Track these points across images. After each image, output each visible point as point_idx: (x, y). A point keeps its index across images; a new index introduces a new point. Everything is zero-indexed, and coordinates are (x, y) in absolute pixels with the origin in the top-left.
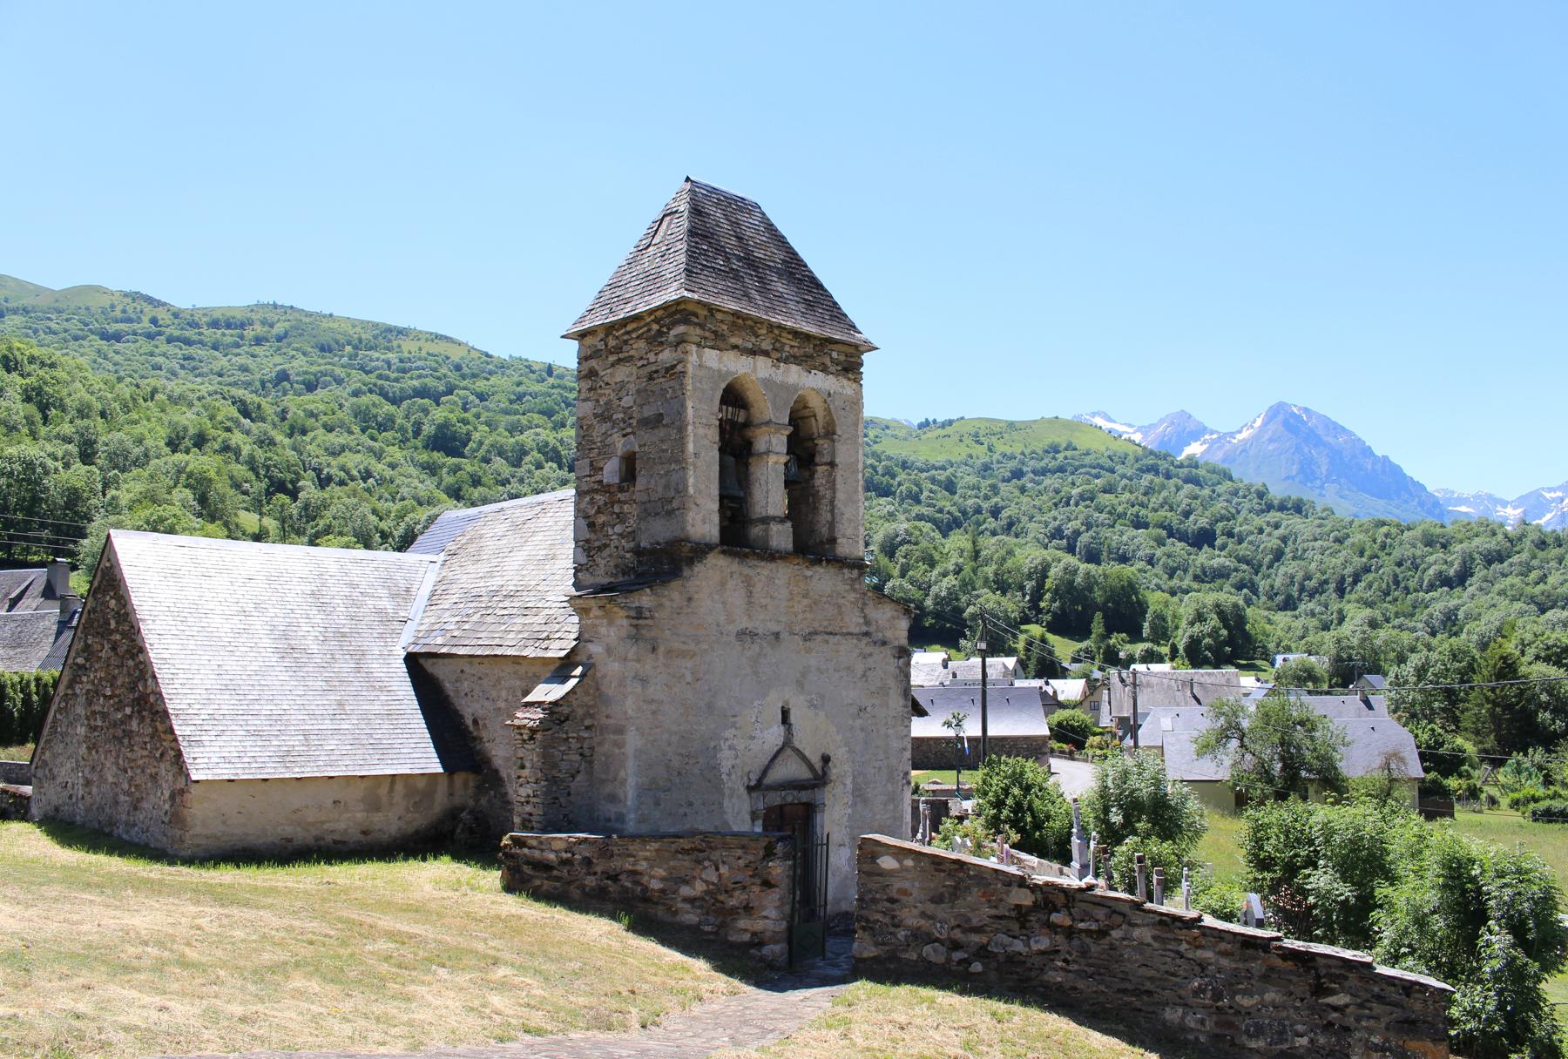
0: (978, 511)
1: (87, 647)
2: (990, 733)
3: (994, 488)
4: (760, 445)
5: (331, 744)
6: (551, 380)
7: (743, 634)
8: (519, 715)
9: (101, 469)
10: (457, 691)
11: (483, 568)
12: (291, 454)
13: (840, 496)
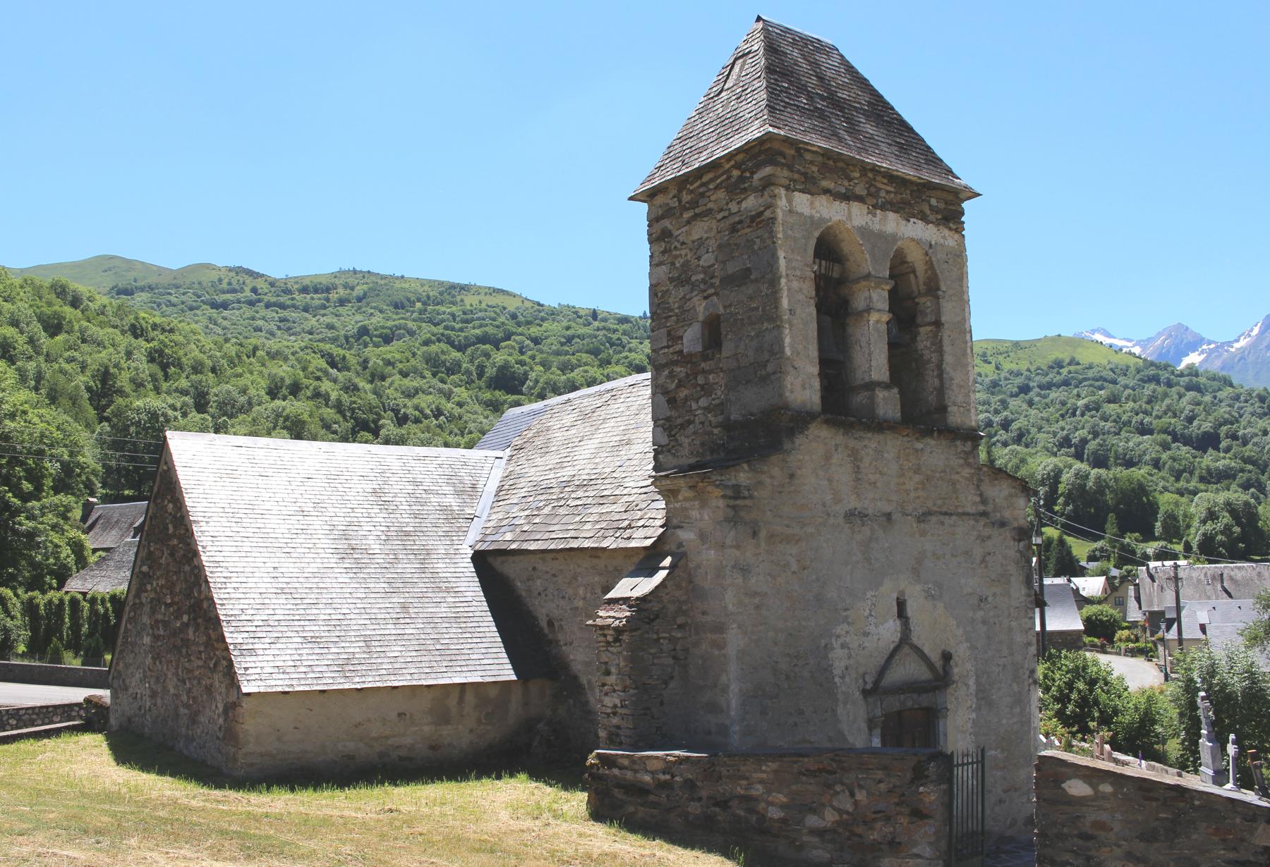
1: (150, 553)
2: (1049, 628)
3: (1003, 402)
4: (859, 302)
5: (395, 650)
6: (596, 324)
7: (851, 515)
8: (601, 613)
9: (213, 417)
10: (529, 591)
11: (552, 460)
12: (371, 397)
13: (949, 359)
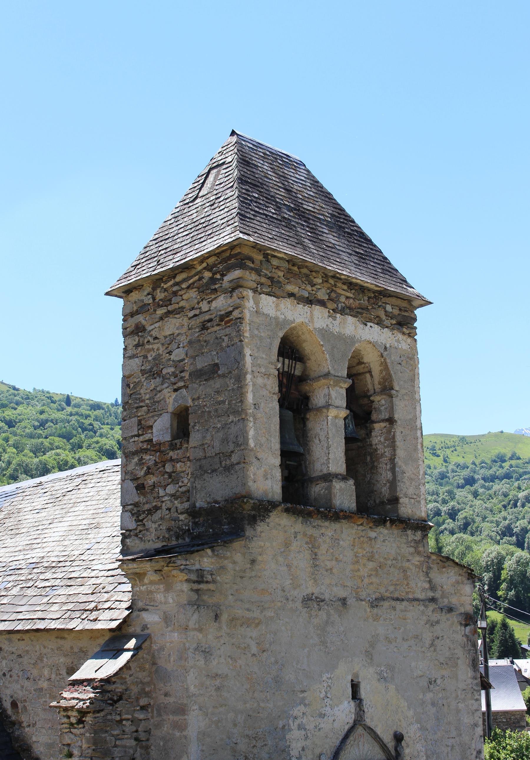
0: (438, 513)
3: (450, 493)
4: (318, 398)
6: (69, 409)
7: (308, 600)
8: (65, 695)
11: (22, 541)
13: (401, 453)
